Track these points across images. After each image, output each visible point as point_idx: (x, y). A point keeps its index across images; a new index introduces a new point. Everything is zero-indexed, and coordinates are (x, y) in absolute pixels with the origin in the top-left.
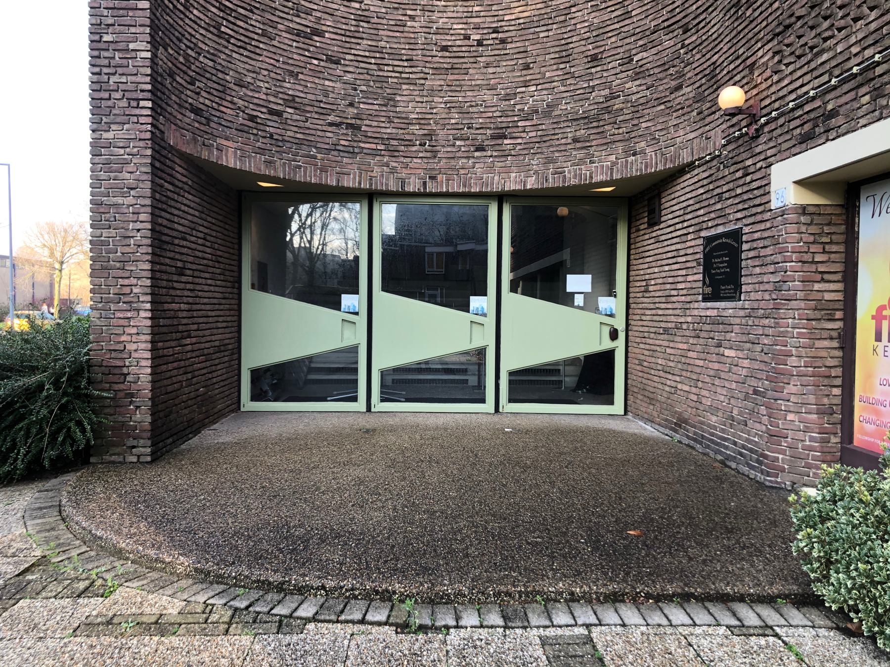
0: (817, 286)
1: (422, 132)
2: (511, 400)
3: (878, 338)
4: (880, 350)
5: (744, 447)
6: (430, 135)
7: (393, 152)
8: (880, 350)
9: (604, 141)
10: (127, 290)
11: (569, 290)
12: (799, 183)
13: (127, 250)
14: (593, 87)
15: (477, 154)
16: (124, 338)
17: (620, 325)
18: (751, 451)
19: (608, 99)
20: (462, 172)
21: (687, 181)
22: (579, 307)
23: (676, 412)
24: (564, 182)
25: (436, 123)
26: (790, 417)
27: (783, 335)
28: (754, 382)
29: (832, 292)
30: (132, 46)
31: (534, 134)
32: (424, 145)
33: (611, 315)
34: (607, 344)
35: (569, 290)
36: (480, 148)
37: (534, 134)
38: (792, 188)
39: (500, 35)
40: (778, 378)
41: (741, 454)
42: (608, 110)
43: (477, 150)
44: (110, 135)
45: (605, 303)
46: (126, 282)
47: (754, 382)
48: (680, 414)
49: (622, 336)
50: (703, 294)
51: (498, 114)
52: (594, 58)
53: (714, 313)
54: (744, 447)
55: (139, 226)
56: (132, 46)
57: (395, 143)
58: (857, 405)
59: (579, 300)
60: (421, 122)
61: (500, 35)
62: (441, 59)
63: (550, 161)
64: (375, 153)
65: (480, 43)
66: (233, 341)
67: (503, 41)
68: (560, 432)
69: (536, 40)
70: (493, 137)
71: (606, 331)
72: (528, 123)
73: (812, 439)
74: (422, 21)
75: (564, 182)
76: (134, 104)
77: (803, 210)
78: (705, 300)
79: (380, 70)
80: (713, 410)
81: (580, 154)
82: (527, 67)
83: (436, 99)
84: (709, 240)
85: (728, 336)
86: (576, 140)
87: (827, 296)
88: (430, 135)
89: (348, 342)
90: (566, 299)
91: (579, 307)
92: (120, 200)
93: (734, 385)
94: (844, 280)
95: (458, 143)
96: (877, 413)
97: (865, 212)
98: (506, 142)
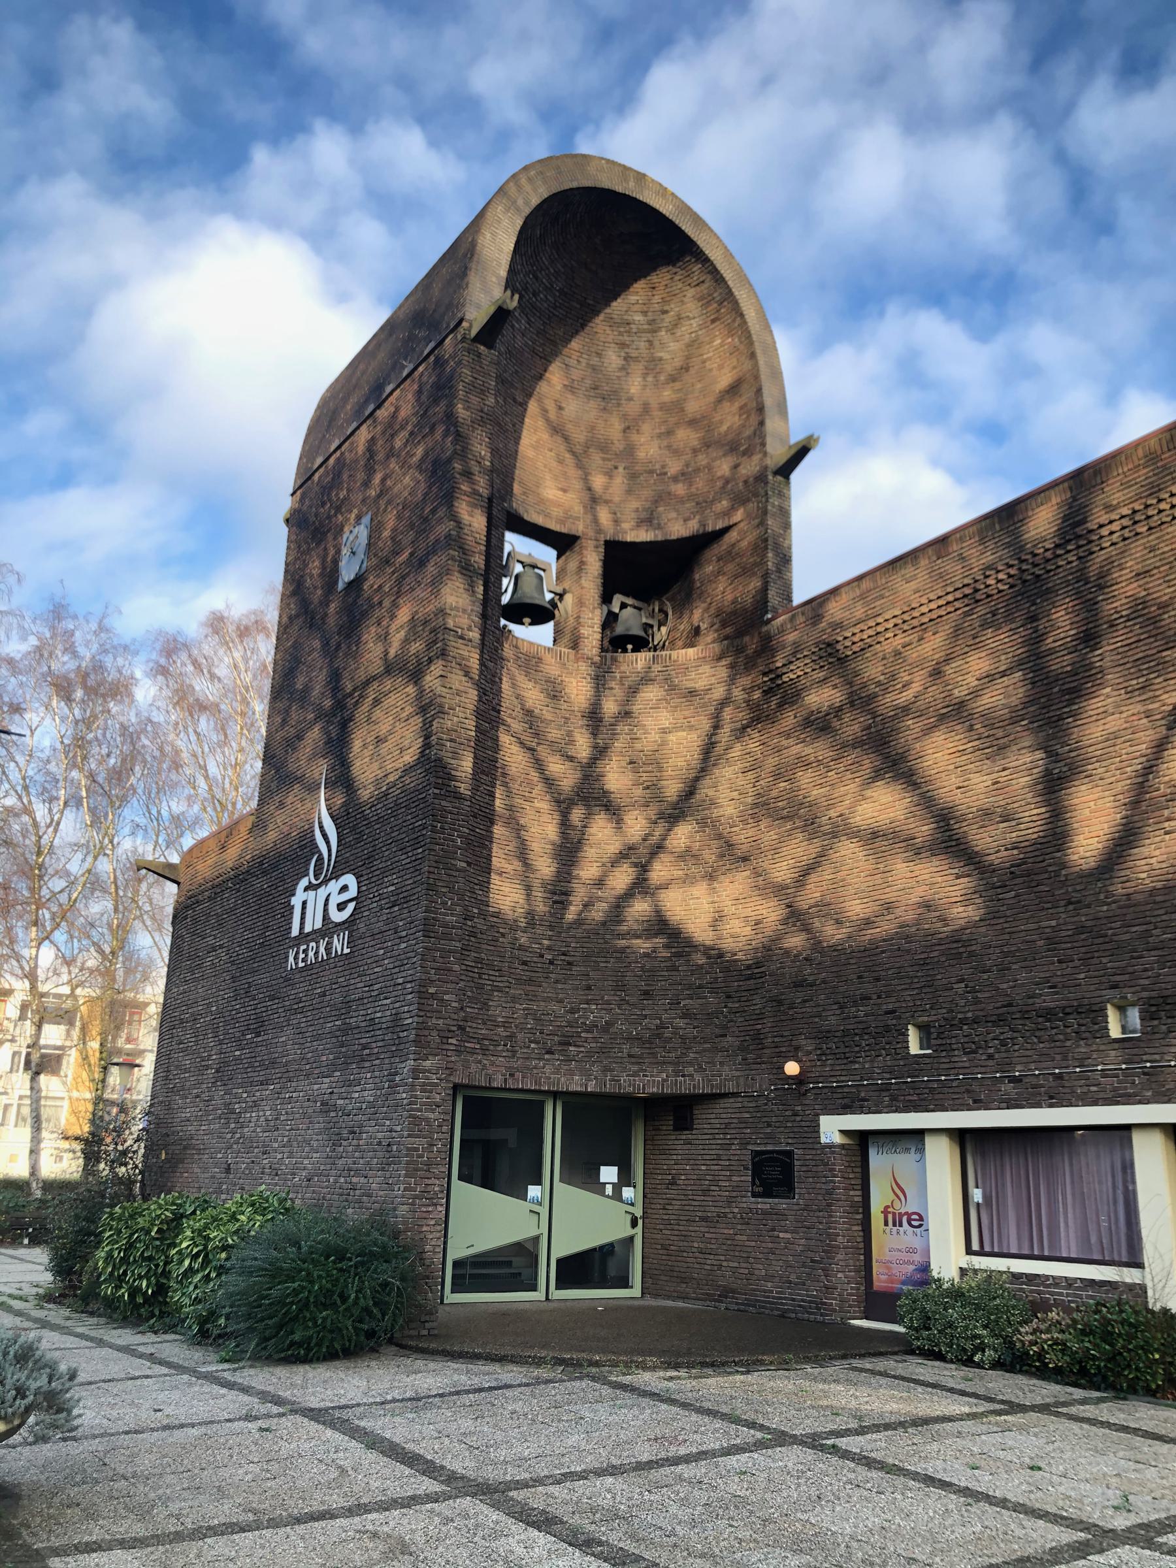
0: (852, 1193)
1: (505, 1034)
2: (557, 1288)
3: (886, 1224)
4: (888, 1231)
5: (803, 1301)
6: (511, 1037)
7: (484, 1050)
8: (888, 1231)
9: (655, 1061)
10: (429, 1188)
11: (602, 1180)
12: (841, 1131)
13: (431, 1155)
14: (646, 1016)
15: (547, 1056)
16: (425, 1229)
17: (639, 1213)
18: (810, 1302)
19: (658, 1028)
20: (535, 1071)
21: (729, 1102)
22: (608, 1197)
23: (720, 1286)
24: (620, 1088)
25: (516, 1027)
26: (840, 1275)
27: (835, 1222)
28: (810, 1254)
29: (856, 1195)
30: (445, 997)
31: (594, 1045)
32: (505, 1045)
33: (632, 1204)
34: (628, 1231)
35: (602, 1180)
36: (550, 1052)
37: (594, 1045)
38: (838, 1133)
39: (567, 958)
40: (830, 1251)
41: (800, 1306)
42: (659, 1036)
43: (547, 1053)
44: (428, 1063)
45: (628, 1193)
46: (430, 1182)
47: (810, 1254)
48: (724, 1286)
49: (640, 1222)
50: (752, 1192)
51: (564, 1024)
52: (646, 993)
53: (768, 1206)
54: (803, 1301)
55: (441, 1136)
56: (445, 997)
57: (486, 1042)
58: (874, 1264)
59: (609, 1190)
60: (505, 1025)
61: (567, 958)
62: (520, 970)
63: (606, 1069)
64: (473, 1052)
65: (551, 963)
66: (439, 1228)
67: (570, 963)
68: (617, 1309)
69: (596, 968)
70: (560, 1043)
71: (629, 1217)
72: (589, 1035)
73: (852, 1288)
74: (509, 938)
75: (620, 1088)
76: (445, 1040)
77: (842, 1146)
78: (754, 1196)
79: (480, 978)
80: (769, 1278)
81: (636, 1068)
82: (589, 988)
83: (517, 1006)
84: (756, 1154)
85: (783, 1223)
86: (630, 1056)
87: (856, 1199)
88: (511, 1037)
89: (533, 1232)
90: (599, 1188)
91: (608, 1197)
92: (431, 1116)
93: (791, 1258)
94: (862, 1189)
95: (533, 1045)
96: (889, 1268)
97: (872, 1153)
98: (571, 1048)
